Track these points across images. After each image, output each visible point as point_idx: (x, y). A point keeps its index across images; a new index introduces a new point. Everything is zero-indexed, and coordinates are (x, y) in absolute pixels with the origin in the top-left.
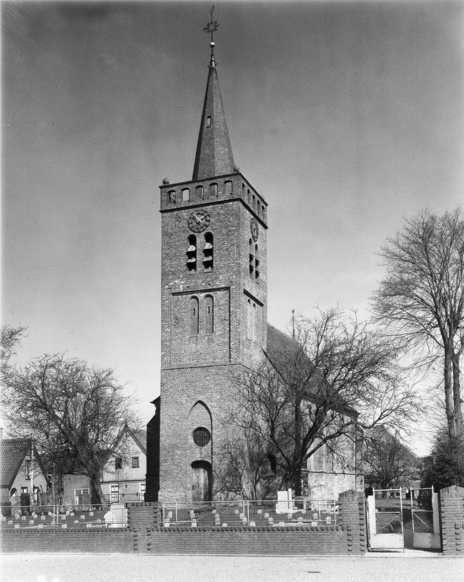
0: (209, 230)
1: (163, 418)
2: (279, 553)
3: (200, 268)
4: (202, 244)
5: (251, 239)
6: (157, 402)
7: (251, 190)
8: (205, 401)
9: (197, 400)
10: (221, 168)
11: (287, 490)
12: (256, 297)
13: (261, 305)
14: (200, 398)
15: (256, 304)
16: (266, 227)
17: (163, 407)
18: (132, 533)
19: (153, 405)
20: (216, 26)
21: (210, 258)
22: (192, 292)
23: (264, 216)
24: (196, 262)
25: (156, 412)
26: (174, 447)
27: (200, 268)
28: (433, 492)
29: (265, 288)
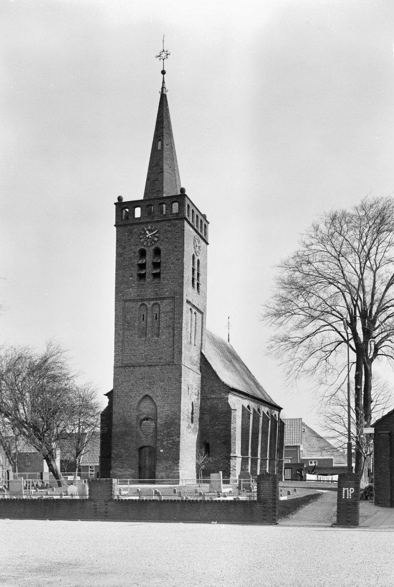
0: (157, 245)
1: (115, 408)
2: (235, 521)
3: (149, 279)
4: (149, 259)
5: (193, 255)
6: (110, 395)
7: (195, 210)
8: (151, 395)
9: (144, 394)
10: (168, 192)
11: (218, 472)
12: (197, 306)
13: (202, 313)
14: (147, 393)
15: (196, 312)
16: (207, 244)
17: (115, 397)
18: (93, 503)
19: (107, 397)
20: (168, 54)
21: (157, 271)
22: (142, 300)
23: (205, 234)
24: (145, 263)
25: (109, 403)
26: (125, 434)
27: (149, 279)
28: (354, 467)
29: (205, 297)
